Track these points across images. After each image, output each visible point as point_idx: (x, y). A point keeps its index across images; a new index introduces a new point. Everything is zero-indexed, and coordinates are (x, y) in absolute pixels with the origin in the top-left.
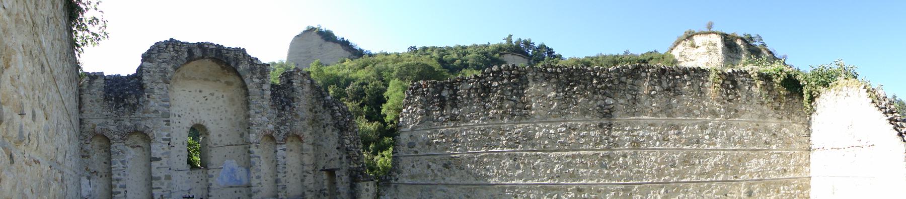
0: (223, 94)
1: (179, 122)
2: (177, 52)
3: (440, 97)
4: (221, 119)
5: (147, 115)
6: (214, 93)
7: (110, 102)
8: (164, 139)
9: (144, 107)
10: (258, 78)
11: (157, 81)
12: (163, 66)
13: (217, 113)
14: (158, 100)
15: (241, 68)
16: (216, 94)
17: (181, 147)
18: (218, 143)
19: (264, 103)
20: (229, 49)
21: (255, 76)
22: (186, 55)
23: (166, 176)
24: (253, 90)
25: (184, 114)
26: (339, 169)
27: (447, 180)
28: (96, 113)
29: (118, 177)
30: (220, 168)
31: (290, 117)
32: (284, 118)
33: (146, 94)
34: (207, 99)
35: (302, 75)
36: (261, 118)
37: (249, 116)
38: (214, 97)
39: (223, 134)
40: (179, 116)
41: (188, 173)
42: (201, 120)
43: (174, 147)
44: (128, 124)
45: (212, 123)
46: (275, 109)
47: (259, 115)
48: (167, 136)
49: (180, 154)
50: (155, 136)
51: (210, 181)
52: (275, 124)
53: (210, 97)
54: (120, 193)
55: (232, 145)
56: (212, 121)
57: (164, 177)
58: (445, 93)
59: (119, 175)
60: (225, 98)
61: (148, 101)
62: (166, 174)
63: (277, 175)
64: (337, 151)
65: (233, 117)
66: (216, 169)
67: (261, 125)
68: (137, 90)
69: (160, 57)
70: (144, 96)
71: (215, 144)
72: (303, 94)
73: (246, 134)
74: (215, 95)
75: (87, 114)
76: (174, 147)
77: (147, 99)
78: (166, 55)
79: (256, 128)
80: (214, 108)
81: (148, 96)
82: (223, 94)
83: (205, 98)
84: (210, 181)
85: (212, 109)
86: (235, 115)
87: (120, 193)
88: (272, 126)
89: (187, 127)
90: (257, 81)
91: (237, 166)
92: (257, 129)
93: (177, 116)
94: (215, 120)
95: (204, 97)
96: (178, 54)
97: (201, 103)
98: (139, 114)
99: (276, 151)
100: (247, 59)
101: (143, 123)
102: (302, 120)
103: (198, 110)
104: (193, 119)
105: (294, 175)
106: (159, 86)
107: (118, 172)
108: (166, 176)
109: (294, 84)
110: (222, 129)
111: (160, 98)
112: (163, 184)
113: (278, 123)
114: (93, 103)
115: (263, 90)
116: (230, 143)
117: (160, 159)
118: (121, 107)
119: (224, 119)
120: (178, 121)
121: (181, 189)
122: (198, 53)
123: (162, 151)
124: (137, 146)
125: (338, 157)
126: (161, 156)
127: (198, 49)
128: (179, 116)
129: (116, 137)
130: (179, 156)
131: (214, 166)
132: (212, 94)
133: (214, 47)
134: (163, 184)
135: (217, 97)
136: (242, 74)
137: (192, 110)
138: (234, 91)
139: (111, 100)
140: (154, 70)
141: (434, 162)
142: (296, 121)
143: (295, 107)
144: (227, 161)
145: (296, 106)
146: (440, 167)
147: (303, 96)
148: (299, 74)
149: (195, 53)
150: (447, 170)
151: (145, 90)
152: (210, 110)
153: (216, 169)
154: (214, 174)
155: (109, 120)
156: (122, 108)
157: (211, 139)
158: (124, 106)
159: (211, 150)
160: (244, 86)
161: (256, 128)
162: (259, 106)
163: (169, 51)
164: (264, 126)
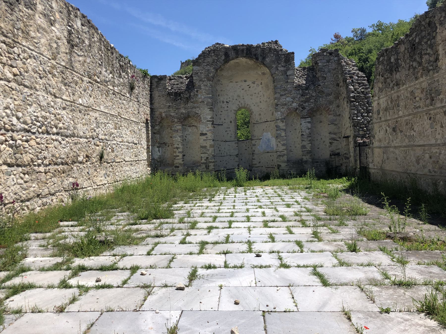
0: (261, 81)
1: (228, 107)
2: (217, 56)
4: (260, 102)
5: (196, 105)
6: (255, 82)
7: (171, 96)
8: (208, 121)
9: (194, 99)
10: (282, 66)
11: (203, 80)
13: (257, 97)
14: (204, 93)
17: (229, 125)
18: (259, 120)
19: (289, 86)
20: (258, 47)
21: (280, 65)
22: (223, 58)
23: (210, 145)
24: (278, 77)
25: (231, 100)
28: (162, 104)
29: (178, 146)
30: (260, 139)
31: (314, 95)
32: (308, 97)
33: (196, 90)
34: (250, 87)
35: (328, 54)
36: (286, 99)
38: (255, 85)
40: (227, 102)
41: (235, 143)
43: (222, 125)
44: (184, 111)
45: (254, 105)
46: (299, 90)
47: (284, 97)
48: (210, 118)
49: (228, 130)
50: (202, 119)
51: (253, 149)
52: (299, 102)
53: (252, 85)
54: (178, 156)
55: (268, 121)
56: (254, 104)
57: (209, 146)
59: (178, 145)
60: (263, 85)
61: (197, 95)
62: (211, 144)
66: (258, 139)
67: (285, 104)
68: (190, 87)
69: (205, 61)
70: (194, 91)
71: (257, 121)
72: (329, 72)
74: (256, 83)
75: (156, 105)
76: (222, 125)
77: (196, 93)
78: (210, 60)
79: (281, 107)
80: (255, 93)
81: (197, 91)
82: (261, 81)
83: (249, 87)
84: (253, 149)
85: (254, 95)
86: (269, 98)
87: (178, 156)
88: (295, 104)
89: (234, 110)
90: (282, 69)
91: (271, 137)
92: (282, 108)
93: (225, 103)
94: (256, 103)
95: (248, 86)
96: (218, 57)
97: (246, 91)
98: (190, 104)
100: (273, 52)
101: (194, 110)
102: (329, 95)
103: (243, 96)
104: (239, 104)
106: (205, 83)
107: (177, 143)
108: (210, 145)
109: (319, 64)
110: (261, 109)
111: (205, 92)
112: (208, 150)
113: (302, 101)
114: (160, 98)
115: (287, 76)
116: (267, 120)
117: (206, 134)
118: (178, 100)
119: (262, 101)
120: (226, 106)
121: (228, 154)
122: (232, 54)
123: (207, 129)
124: (193, 126)
126: (206, 132)
127: (233, 52)
128: (227, 102)
129: (176, 120)
130: (227, 131)
131: (256, 138)
132: (254, 83)
133: (245, 47)
134: (208, 150)
135: (258, 85)
137: (239, 96)
139: (172, 95)
140: (200, 71)
142: (320, 97)
143: (320, 85)
144: (265, 134)
145: (321, 84)
147: (329, 74)
148: (325, 54)
149: (230, 55)
151: (195, 87)
152: (252, 95)
153: (258, 139)
154: (256, 143)
155: (171, 109)
156: (180, 100)
158: (181, 99)
161: (281, 107)
162: (283, 90)
163: (211, 56)
164: (288, 106)
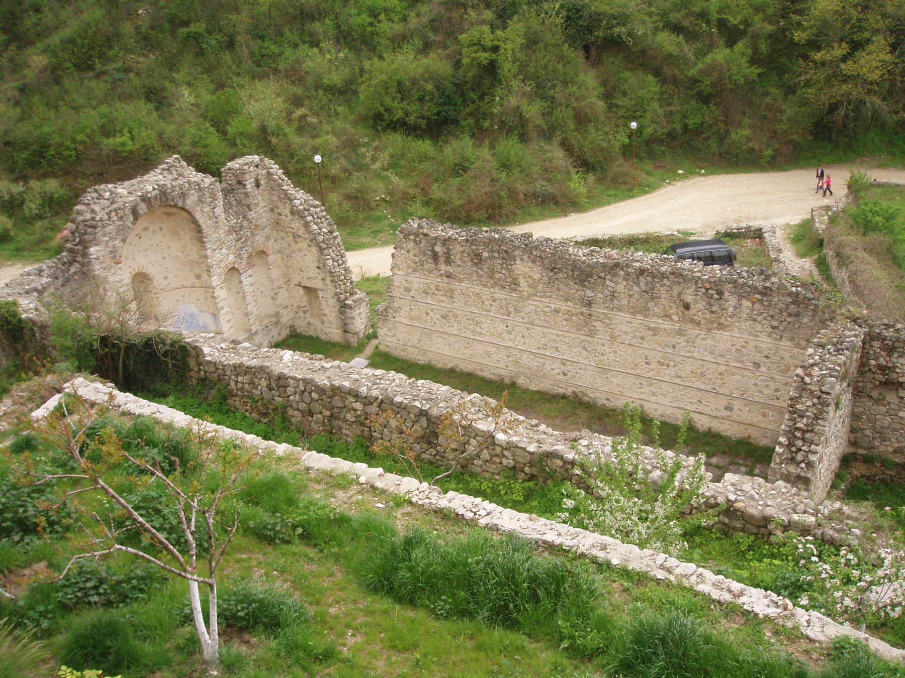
3: (433, 251)
12: (111, 244)
15: (190, 202)
16: (151, 227)
26: (322, 290)
27: (446, 329)
37: (206, 257)
38: (150, 232)
39: (169, 275)
42: (139, 268)
53: (143, 234)
58: (438, 248)
63: (246, 308)
64: (318, 270)
65: (180, 254)
71: (162, 290)
73: (205, 276)
86: (183, 252)
99: (241, 282)
105: (262, 292)
125: (320, 277)
136: (190, 210)
138: (187, 235)
141: (432, 310)
146: (439, 316)
150: (445, 321)
157: (156, 285)
159: (158, 298)
160: (195, 222)
